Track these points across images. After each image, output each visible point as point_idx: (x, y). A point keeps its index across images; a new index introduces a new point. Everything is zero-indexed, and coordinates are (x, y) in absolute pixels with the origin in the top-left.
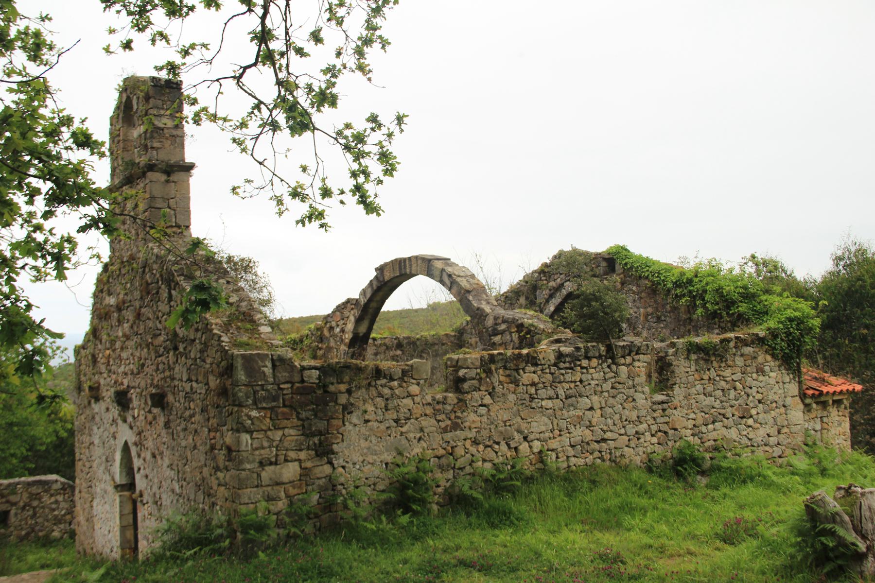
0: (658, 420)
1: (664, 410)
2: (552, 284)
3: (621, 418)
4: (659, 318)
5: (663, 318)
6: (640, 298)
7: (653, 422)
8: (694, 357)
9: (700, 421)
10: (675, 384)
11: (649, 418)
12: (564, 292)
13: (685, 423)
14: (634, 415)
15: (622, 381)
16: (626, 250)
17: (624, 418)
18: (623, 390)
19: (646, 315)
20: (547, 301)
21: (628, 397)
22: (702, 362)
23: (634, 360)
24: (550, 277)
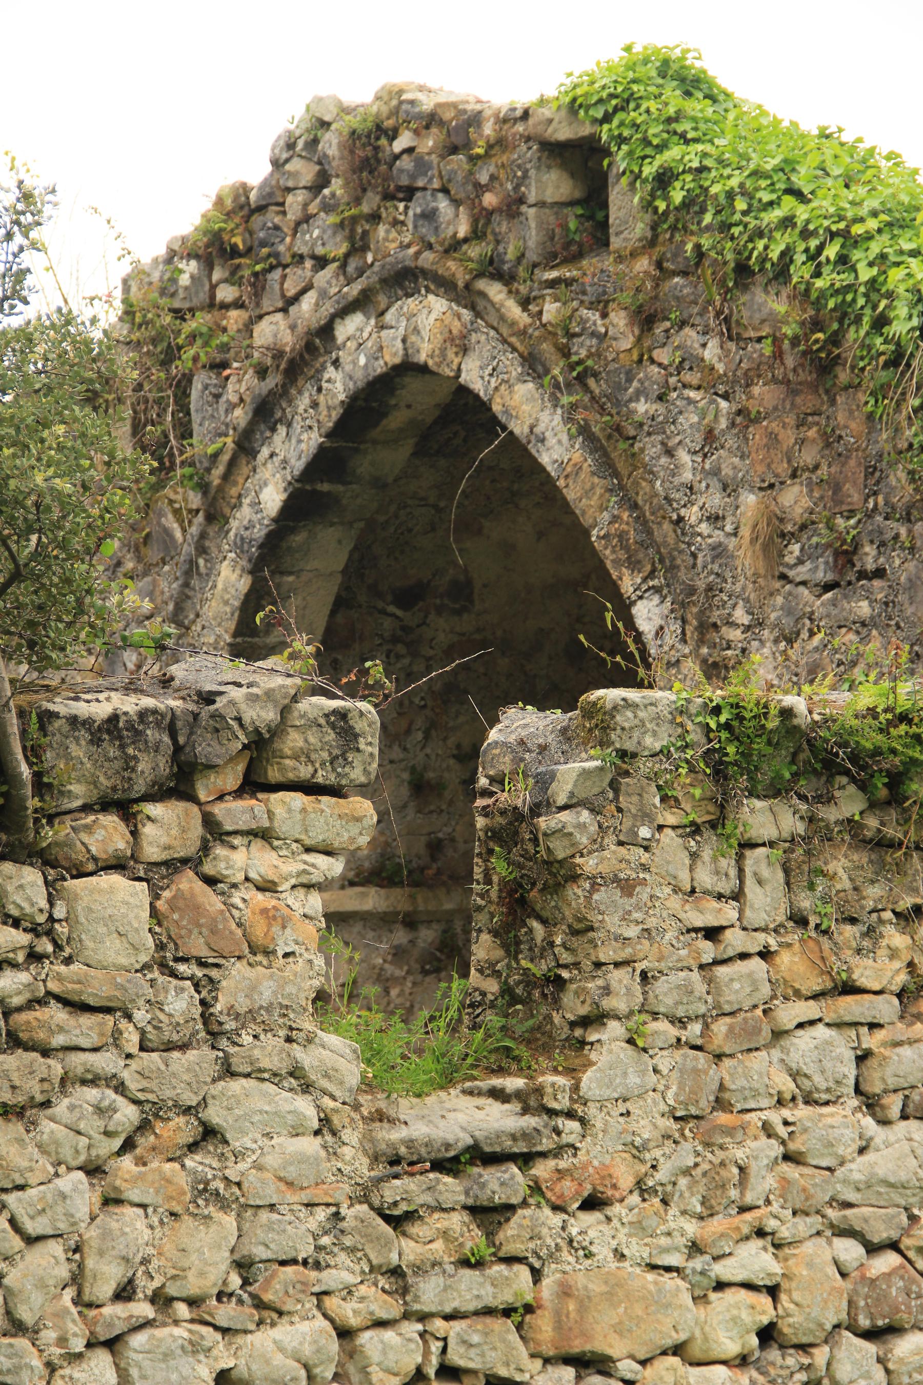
0: (429, 1293)
1: (489, 1214)
2: (274, 331)
3: (77, 1279)
4: (845, 555)
5: (869, 557)
6: (745, 418)
7: (389, 1308)
8: (761, 818)
9: (814, 1303)
10: (596, 1019)
11: (341, 1273)
12: (337, 385)
13: (681, 1316)
14: (205, 1253)
15: (98, 989)
16: (692, 83)
17: (106, 1276)
18: (106, 1062)
19: (776, 535)
20: (246, 447)
21: (152, 1114)
22: (841, 865)
23: (215, 833)
24: (258, 283)
